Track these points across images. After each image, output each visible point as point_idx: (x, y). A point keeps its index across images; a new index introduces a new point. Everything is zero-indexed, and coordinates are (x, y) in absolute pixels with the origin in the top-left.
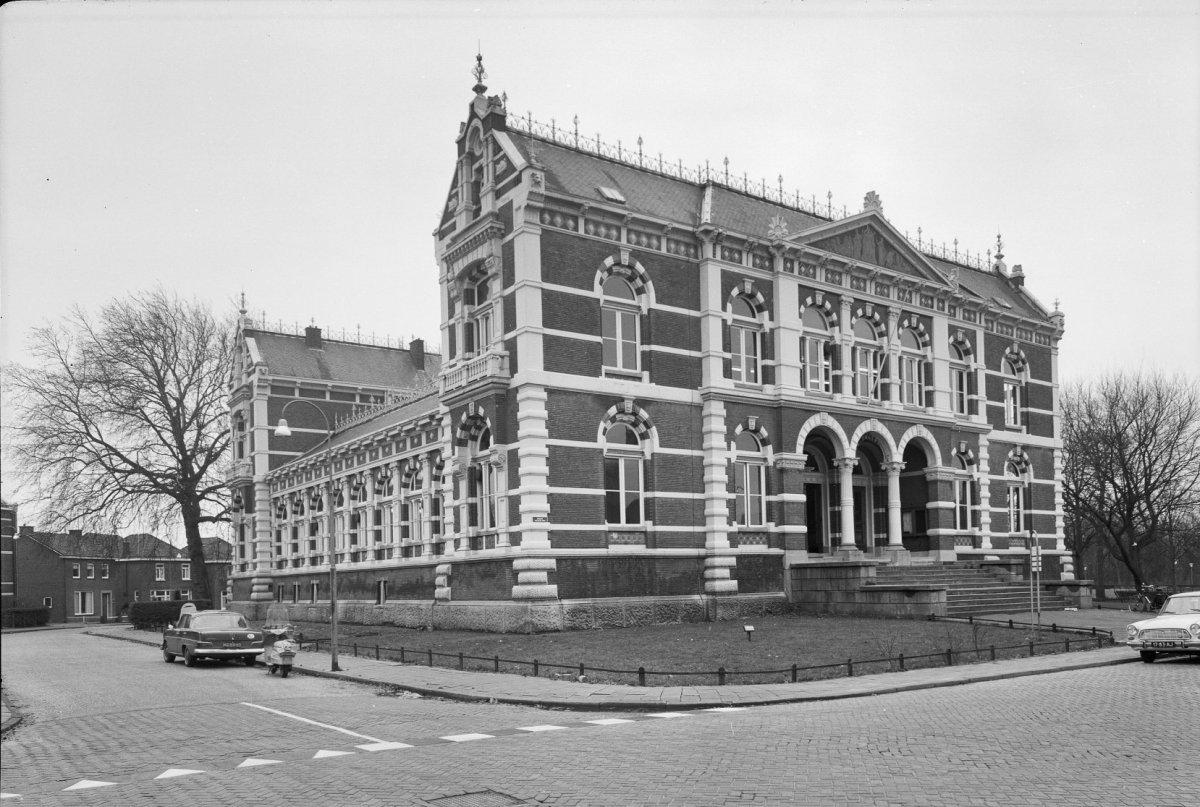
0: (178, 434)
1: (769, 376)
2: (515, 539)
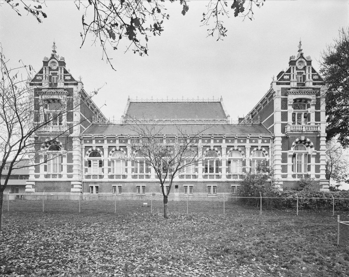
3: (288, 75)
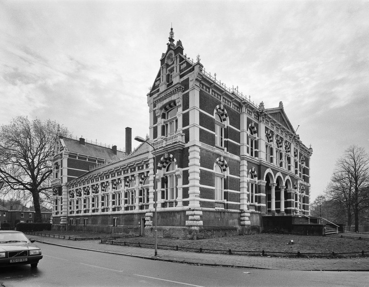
0: (32, 172)
1: (257, 154)
2: (186, 203)
3: (184, 63)
